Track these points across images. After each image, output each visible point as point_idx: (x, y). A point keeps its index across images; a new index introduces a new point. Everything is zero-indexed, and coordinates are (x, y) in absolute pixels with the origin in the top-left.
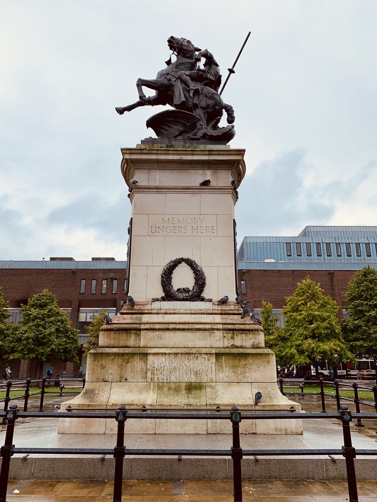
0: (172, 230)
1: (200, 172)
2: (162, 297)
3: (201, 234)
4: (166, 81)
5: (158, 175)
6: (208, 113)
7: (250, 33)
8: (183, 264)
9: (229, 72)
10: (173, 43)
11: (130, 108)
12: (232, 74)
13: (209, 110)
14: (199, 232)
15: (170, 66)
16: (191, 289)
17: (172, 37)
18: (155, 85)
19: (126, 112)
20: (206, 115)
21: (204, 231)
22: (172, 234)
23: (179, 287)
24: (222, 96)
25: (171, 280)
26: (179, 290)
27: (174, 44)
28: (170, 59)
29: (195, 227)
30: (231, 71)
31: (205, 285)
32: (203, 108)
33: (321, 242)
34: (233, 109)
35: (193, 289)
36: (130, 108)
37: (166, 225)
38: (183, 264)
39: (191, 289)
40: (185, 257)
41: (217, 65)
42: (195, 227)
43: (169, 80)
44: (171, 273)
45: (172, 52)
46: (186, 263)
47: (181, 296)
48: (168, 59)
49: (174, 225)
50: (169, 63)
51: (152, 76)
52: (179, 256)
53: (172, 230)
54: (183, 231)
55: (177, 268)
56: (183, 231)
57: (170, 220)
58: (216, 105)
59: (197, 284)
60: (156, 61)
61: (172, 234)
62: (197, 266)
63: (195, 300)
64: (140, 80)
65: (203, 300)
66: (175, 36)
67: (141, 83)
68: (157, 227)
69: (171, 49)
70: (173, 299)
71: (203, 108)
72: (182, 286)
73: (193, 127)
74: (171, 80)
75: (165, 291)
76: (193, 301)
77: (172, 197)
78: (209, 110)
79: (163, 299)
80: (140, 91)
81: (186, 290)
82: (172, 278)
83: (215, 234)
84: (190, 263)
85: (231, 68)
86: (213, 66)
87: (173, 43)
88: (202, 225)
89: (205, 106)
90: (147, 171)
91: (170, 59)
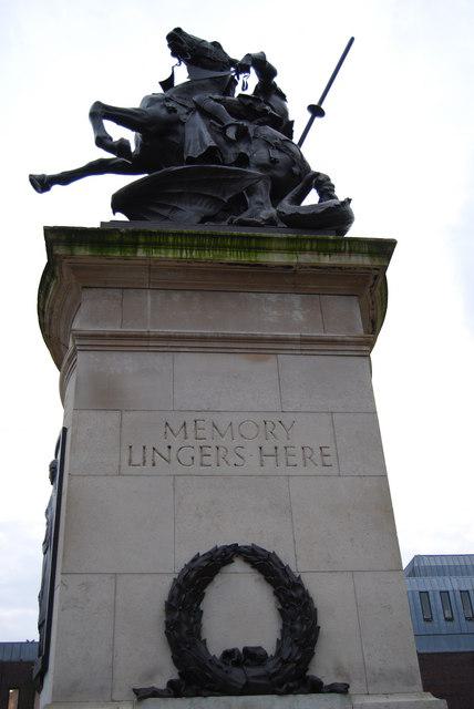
0: (197, 458)
1: (273, 298)
2: (171, 684)
3: (291, 471)
4: (164, 112)
5: (149, 297)
6: (274, 179)
7: (352, 39)
8: (238, 566)
9: (309, 115)
10: (179, 43)
11: (66, 178)
12: (317, 119)
13: (275, 172)
14: (283, 465)
15: (171, 91)
16: (270, 649)
17: (178, 30)
18: (137, 119)
19: (56, 188)
20: (270, 184)
21: (298, 460)
22: (196, 469)
23: (230, 647)
24: (303, 149)
25: (198, 621)
26: (228, 654)
27: (182, 43)
28: (172, 75)
29: (268, 449)
30: (316, 111)
31: (317, 636)
32: (261, 167)
33: (450, 589)
34: (333, 182)
35: (279, 652)
36: (66, 178)
37: (176, 442)
38: (238, 566)
39: (270, 649)
40: (244, 541)
41: (283, 97)
42: (268, 449)
43: (173, 110)
44: (199, 596)
45: (176, 61)
46: (247, 560)
47: (238, 676)
48: (166, 77)
49: (202, 443)
50: (167, 84)
51: (131, 100)
52: (223, 541)
53: (197, 458)
54: (233, 459)
55: (218, 580)
56: (232, 461)
57: (190, 427)
58: (294, 163)
59: (293, 631)
60: (144, 73)
61: (196, 469)
62: (286, 570)
63: (289, 691)
64: (98, 105)
65: (316, 687)
66: (186, 29)
67: (100, 113)
68: (149, 451)
69: (174, 54)
70: (208, 689)
71: (261, 167)
72: (239, 643)
73: (239, 203)
74: (175, 111)
75: (178, 660)
76: (280, 694)
77: (189, 364)
78: (275, 172)
79: (175, 690)
80: (98, 126)
81: (252, 656)
82: (169, 46)
83: (335, 472)
84: (265, 564)
85: (316, 103)
86: (275, 98)
87: (179, 43)
88: (289, 443)
89: (267, 162)
90: (117, 293)
91: (172, 75)
